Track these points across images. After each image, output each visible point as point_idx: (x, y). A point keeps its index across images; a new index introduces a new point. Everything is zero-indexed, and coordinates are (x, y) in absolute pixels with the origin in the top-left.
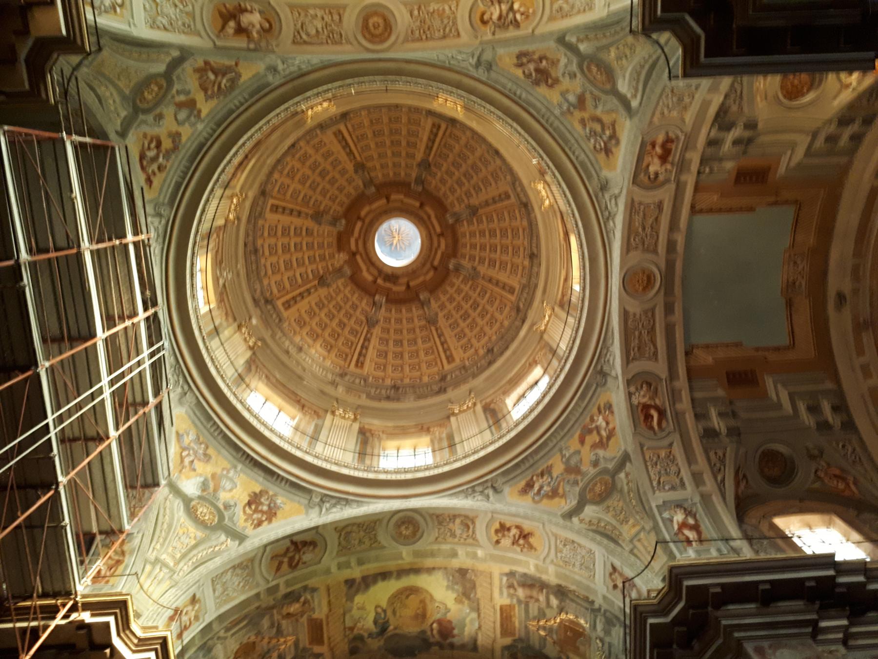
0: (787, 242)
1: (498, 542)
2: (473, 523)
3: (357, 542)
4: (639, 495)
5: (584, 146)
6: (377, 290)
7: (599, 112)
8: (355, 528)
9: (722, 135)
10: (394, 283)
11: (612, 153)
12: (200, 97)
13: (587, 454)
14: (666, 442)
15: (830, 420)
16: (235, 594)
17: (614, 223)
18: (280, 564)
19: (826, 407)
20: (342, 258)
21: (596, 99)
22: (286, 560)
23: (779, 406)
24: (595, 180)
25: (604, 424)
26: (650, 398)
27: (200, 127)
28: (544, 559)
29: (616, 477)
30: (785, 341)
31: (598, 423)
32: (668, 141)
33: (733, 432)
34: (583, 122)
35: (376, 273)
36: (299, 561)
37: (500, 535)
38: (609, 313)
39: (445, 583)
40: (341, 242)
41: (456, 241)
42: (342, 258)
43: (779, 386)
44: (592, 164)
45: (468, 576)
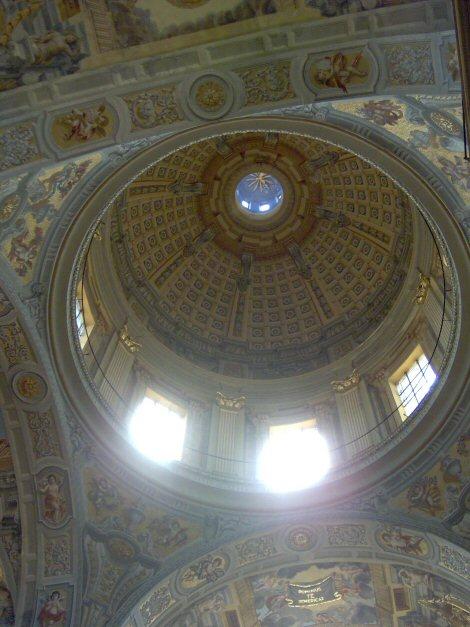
1: (102, 109)
2: (134, 122)
3: (268, 77)
6: (275, 149)
8: (272, 95)
10: (258, 155)
12: (440, 483)
13: (31, 224)
16: (407, 48)
18: (355, 65)
20: (317, 179)
22: (350, 68)
25: (21, 256)
27: (442, 454)
28: (46, 116)
32: (51, 514)
35: (279, 164)
36: (335, 61)
37: (102, 119)
39: (153, 19)
40: (318, 196)
41: (201, 213)
42: (317, 179)
45: (126, 37)
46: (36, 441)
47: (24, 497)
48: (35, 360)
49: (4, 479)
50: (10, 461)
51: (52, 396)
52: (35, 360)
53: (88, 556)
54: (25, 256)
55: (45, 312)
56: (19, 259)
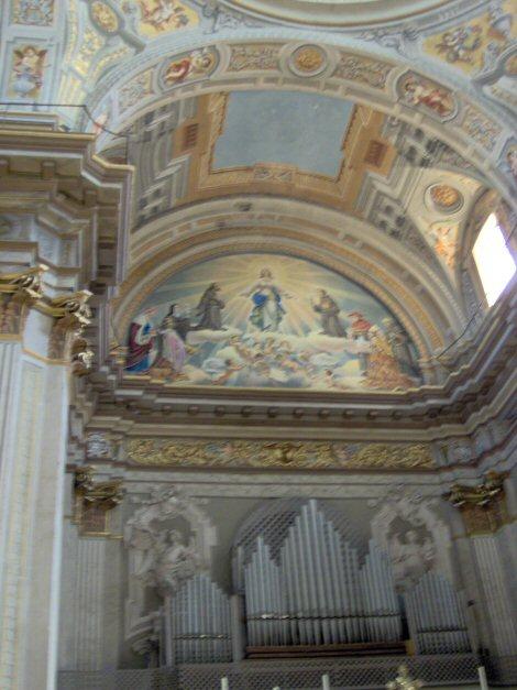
0: (303, 170)
4: (111, 68)
5: (455, 22)
7: (483, 49)
9: (425, 142)
11: (440, 52)
14: (155, 88)
15: (148, 206)
17: (370, 40)
19: (158, 202)
21: (497, 52)
23: (163, 167)
24: (415, 27)
25: (165, 16)
26: (194, 68)
29: (118, 37)
30: (216, 166)
31: (165, 9)
32: (442, 109)
33: (147, 137)
34: (477, 29)
38: (280, 25)
43: (180, 166)
44: (432, 27)
46: (366, 81)
47: (415, 120)
48: (281, 44)
49: (392, 126)
50: (378, 114)
51: (327, 45)
52: (281, 44)
53: (502, 101)
54: (168, 11)
55: (238, 12)
56: (167, 20)
